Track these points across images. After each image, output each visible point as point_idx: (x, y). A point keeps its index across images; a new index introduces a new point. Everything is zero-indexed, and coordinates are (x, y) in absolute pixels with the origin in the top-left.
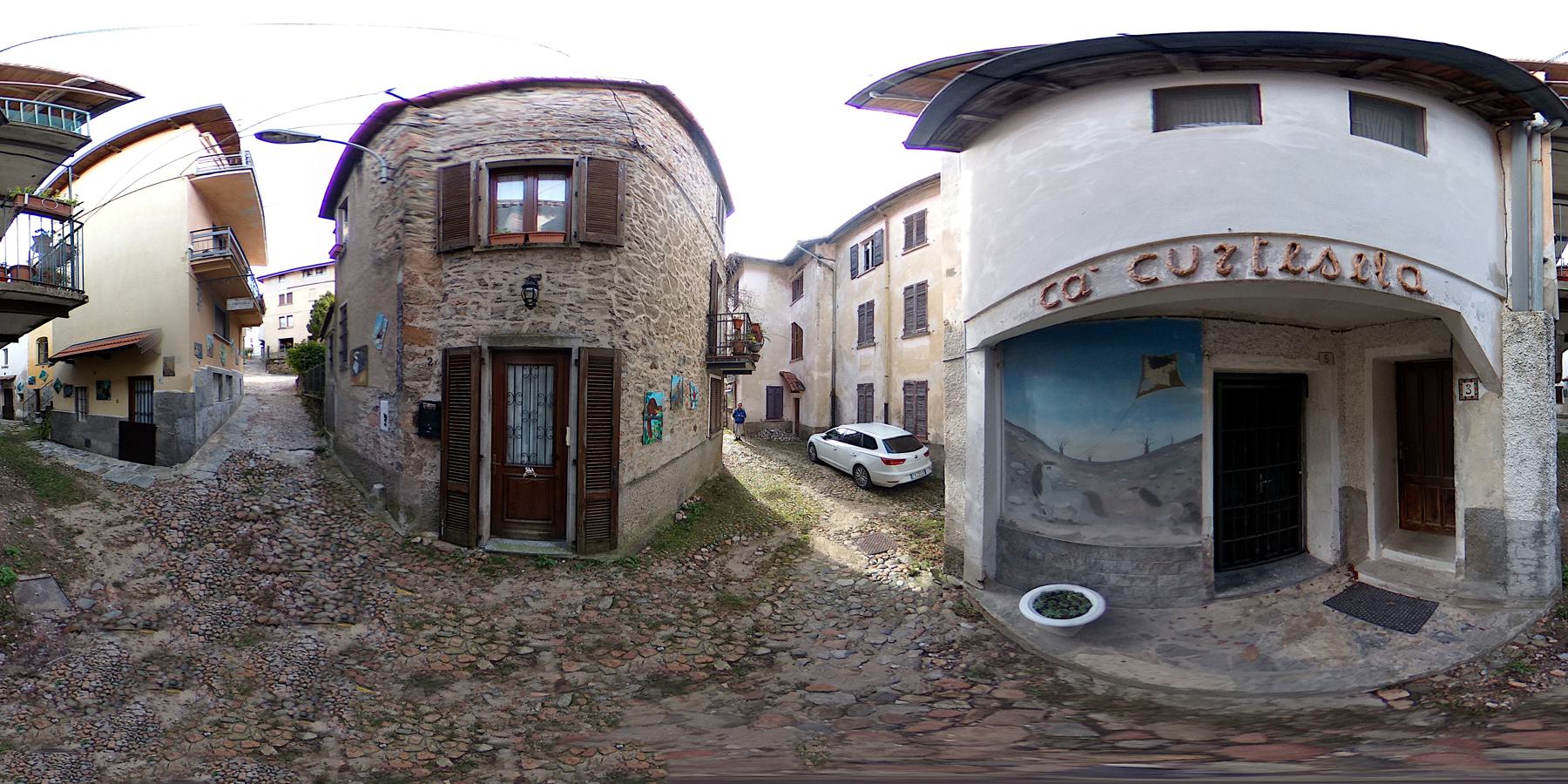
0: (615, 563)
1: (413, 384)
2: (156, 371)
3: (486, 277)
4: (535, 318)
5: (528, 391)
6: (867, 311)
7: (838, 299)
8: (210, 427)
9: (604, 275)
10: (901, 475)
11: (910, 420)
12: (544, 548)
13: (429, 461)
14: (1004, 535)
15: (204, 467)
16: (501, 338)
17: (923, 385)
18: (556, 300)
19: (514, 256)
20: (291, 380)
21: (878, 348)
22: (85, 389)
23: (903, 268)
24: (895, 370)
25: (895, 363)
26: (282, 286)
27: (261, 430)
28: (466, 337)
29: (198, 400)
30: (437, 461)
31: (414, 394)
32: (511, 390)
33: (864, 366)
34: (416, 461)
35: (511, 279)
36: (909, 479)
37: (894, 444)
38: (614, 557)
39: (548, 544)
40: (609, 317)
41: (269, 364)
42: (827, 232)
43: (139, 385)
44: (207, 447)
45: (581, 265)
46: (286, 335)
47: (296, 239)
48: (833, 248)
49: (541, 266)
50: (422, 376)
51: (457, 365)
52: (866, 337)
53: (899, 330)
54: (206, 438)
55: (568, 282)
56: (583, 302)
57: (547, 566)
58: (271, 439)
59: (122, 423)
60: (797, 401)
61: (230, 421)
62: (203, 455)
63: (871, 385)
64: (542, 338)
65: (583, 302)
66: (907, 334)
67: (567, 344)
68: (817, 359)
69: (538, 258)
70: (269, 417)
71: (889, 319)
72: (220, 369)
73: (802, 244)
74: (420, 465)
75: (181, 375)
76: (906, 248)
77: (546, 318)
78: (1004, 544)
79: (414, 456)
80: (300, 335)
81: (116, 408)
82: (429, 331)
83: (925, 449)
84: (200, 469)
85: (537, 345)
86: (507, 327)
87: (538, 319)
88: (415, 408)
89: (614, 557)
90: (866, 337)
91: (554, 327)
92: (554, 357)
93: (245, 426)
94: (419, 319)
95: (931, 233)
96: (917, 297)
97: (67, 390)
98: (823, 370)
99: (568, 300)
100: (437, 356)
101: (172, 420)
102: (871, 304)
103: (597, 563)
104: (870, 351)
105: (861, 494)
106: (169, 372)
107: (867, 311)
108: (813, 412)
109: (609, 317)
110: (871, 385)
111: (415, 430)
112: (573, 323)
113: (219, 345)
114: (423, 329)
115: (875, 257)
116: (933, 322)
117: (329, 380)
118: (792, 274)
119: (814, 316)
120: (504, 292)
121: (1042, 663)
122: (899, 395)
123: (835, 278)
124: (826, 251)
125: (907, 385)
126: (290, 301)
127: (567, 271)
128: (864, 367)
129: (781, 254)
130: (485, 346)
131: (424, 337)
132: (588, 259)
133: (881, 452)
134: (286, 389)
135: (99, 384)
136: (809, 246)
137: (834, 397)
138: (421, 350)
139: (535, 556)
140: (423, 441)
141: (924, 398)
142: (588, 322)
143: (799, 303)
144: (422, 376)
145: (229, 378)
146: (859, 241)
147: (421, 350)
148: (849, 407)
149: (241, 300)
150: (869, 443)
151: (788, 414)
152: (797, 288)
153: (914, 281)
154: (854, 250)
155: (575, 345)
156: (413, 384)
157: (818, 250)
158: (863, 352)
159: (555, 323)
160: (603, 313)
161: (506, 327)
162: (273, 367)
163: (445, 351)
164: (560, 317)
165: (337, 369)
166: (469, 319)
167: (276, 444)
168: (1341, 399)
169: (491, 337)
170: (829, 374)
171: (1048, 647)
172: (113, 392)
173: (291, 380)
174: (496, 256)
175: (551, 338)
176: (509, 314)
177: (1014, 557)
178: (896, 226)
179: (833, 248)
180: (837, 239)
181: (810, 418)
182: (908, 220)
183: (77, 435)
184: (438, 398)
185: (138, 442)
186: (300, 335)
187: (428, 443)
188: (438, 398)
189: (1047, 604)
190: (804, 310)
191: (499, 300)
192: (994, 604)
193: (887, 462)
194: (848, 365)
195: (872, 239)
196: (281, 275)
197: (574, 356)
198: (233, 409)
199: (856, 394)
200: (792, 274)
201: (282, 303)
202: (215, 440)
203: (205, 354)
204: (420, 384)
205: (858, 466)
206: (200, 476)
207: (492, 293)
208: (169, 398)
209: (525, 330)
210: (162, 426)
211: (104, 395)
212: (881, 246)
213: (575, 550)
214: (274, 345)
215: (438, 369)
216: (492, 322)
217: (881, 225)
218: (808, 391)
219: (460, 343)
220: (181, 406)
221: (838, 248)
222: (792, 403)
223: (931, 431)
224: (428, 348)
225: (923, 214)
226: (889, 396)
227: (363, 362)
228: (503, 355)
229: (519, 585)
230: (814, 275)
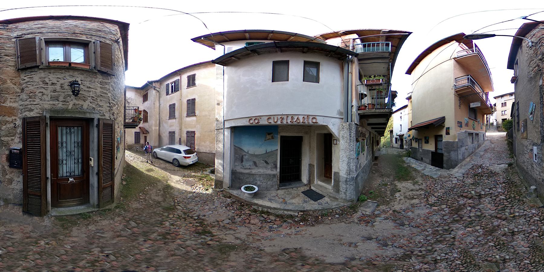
0: (116, 207)
1: (6, 139)
2: (444, 132)
3: (47, 80)
4: (75, 101)
5: (69, 140)
6: (172, 107)
7: (161, 102)
8: (466, 154)
9: (106, 86)
10: (189, 161)
11: (189, 144)
12: (81, 209)
13: (16, 179)
14: (234, 173)
15: (460, 171)
16: (57, 111)
17: (194, 132)
18: (86, 94)
19: (63, 71)
20: (504, 134)
21: (177, 120)
22: (421, 139)
23: (186, 93)
24: (183, 127)
25: (183, 125)
26: (503, 100)
27: (488, 155)
28: (36, 111)
29: (460, 144)
30: (21, 179)
31: (7, 144)
32: (60, 140)
33: (172, 125)
34: (8, 179)
35: (62, 81)
36: (192, 163)
37: (187, 152)
38: (114, 205)
39: (82, 207)
40: (109, 105)
41: (498, 128)
42: (158, 78)
43: (438, 138)
44: (464, 163)
45: (97, 80)
46: (504, 117)
47: (501, 82)
48: (159, 84)
49: (79, 78)
50: (10, 134)
51: (31, 127)
52: (172, 115)
53: (185, 114)
54: (464, 159)
55: (91, 85)
56: (98, 97)
57: (90, 217)
58: (491, 159)
59: (432, 152)
60: (146, 137)
61: (477, 151)
62: (462, 165)
63: (174, 132)
64: (80, 112)
65: (98, 97)
66: (188, 115)
67: (92, 116)
68: (154, 123)
69: (76, 73)
70: (493, 149)
71: (182, 109)
72: (472, 131)
73: (149, 82)
74: (11, 181)
75: (453, 133)
76: (188, 87)
77: (81, 102)
78: (234, 176)
79: (7, 177)
80: (508, 116)
81: (431, 147)
82: (14, 108)
83: (195, 153)
84: (457, 172)
85: (77, 116)
86: (60, 105)
87: (77, 102)
88: (7, 152)
89: (114, 205)
90: (172, 115)
91: (85, 107)
92: (84, 124)
93: (482, 153)
94: (8, 102)
95: (197, 82)
96: (192, 103)
97: (417, 140)
98: (156, 126)
99: (91, 94)
100: (19, 122)
101: (449, 152)
102: (174, 104)
103: (109, 210)
104: (174, 120)
105: (176, 168)
106: (448, 133)
107: (172, 107)
108: (152, 140)
109: (109, 105)
110: (174, 132)
111: (7, 164)
112: (94, 106)
113: (471, 122)
114: (10, 107)
115: (176, 88)
116: (197, 112)
117: (514, 135)
118: (143, 93)
119: (153, 108)
120: (58, 87)
121: (249, 205)
122: (184, 135)
123: (160, 94)
124: (157, 85)
125: (188, 132)
126: (505, 105)
127: (90, 81)
128: (171, 126)
129: (140, 85)
130: (48, 116)
131: (11, 111)
132: (100, 78)
133: (183, 154)
134: (502, 138)
135: (425, 138)
136: (151, 83)
137: (160, 136)
138: (10, 119)
139: (80, 214)
140: (12, 170)
141: (194, 137)
142: (100, 106)
143: (146, 103)
144: (10, 134)
145: (477, 134)
146: (171, 82)
147: (10, 119)
148: (166, 138)
149: (476, 103)
150: (179, 152)
151: (142, 141)
152: (145, 98)
153: (191, 98)
154: (168, 85)
155: (96, 117)
156: (6, 139)
157: (154, 85)
158: (171, 121)
159: (86, 105)
160: (106, 103)
161: (60, 105)
162: (499, 129)
163: (24, 119)
164: (88, 102)
165: (516, 130)
166: (37, 101)
167: (493, 161)
168: (181, 105)
169: (51, 111)
170: (158, 128)
171: (249, 200)
172: (430, 140)
173: (504, 134)
174: (52, 71)
175: (85, 113)
176: (61, 99)
177: (237, 179)
178: (184, 79)
179: (159, 84)
180: (161, 81)
181: (152, 144)
182: (189, 77)
183: (419, 156)
184: (20, 146)
185: (437, 160)
186: (508, 116)
187: (15, 170)
188: (20, 146)
189: (247, 189)
190: (148, 105)
191: (55, 91)
192: (235, 192)
193: (185, 157)
194: (165, 125)
195: (175, 82)
196: (502, 96)
197: (96, 123)
198: (479, 146)
199: (168, 135)
200: (143, 93)
201: (502, 106)
202: (468, 159)
203: (463, 125)
204: (10, 139)
205: (175, 159)
206: (457, 175)
207: (51, 88)
208: (448, 143)
209: (70, 107)
210: (445, 154)
211: (427, 142)
212: (178, 85)
213: (99, 207)
214: (500, 121)
215: (20, 130)
216: (51, 102)
217: (178, 78)
218: (150, 133)
219: (32, 114)
220: (452, 147)
221: (161, 84)
222: (144, 138)
223: (196, 147)
224: (14, 118)
225: (194, 75)
226: (181, 136)
227: (525, 126)
228: (59, 121)
229: (92, 227)
230: (152, 94)
